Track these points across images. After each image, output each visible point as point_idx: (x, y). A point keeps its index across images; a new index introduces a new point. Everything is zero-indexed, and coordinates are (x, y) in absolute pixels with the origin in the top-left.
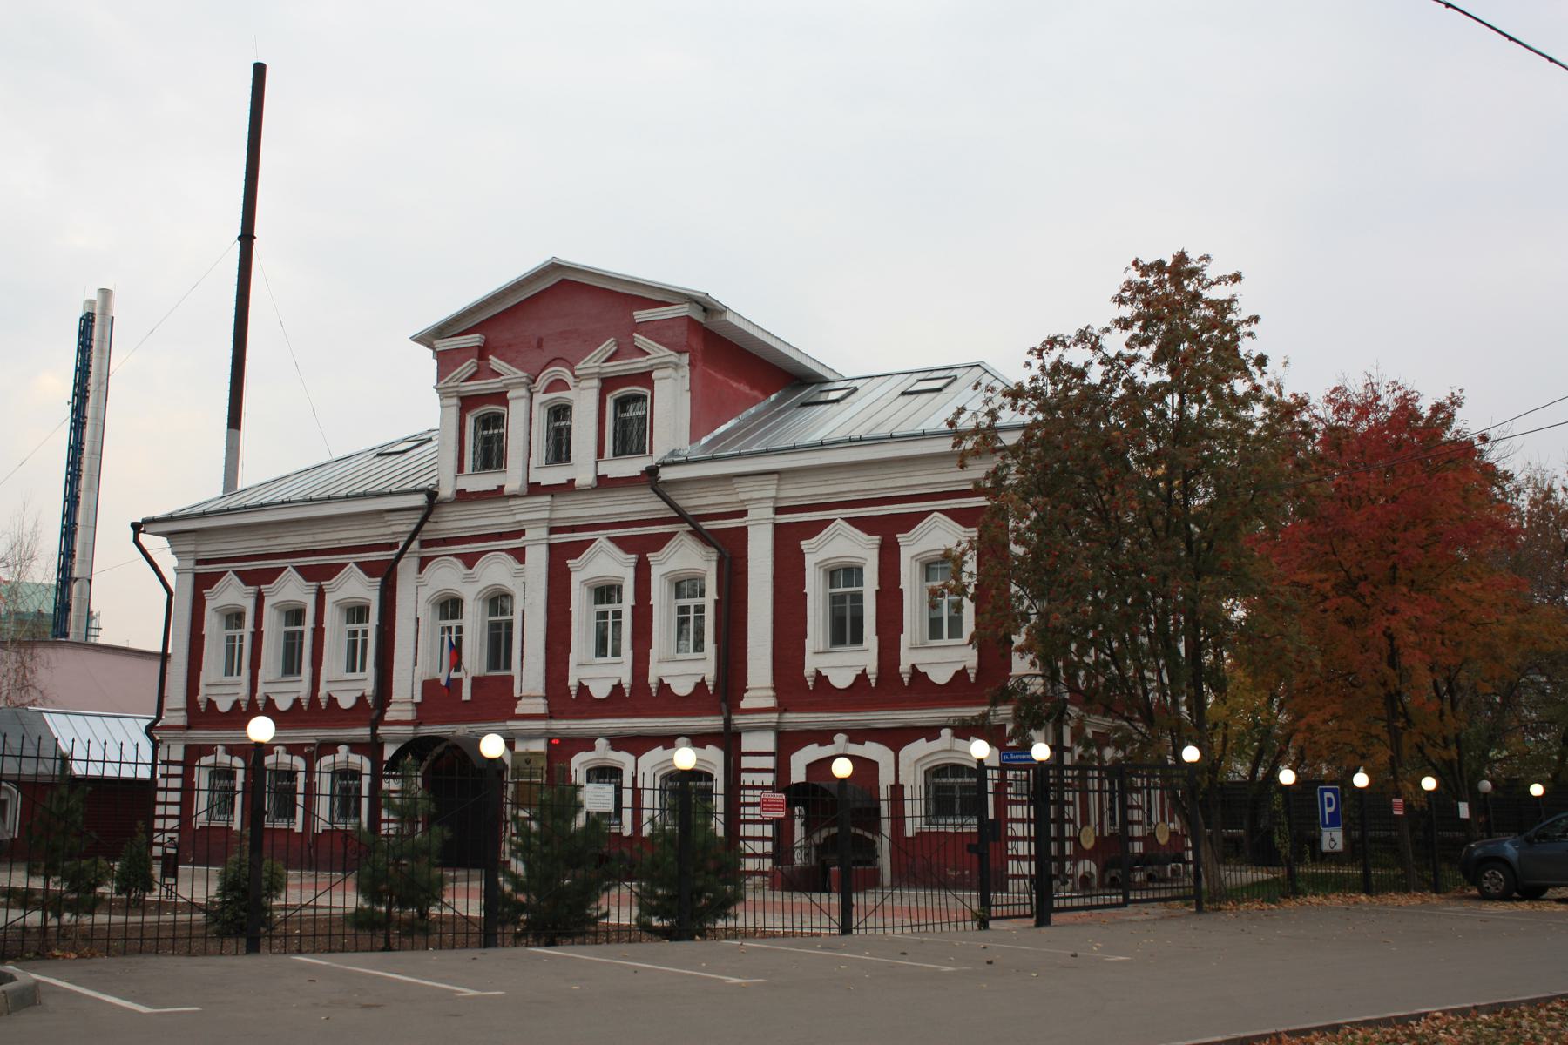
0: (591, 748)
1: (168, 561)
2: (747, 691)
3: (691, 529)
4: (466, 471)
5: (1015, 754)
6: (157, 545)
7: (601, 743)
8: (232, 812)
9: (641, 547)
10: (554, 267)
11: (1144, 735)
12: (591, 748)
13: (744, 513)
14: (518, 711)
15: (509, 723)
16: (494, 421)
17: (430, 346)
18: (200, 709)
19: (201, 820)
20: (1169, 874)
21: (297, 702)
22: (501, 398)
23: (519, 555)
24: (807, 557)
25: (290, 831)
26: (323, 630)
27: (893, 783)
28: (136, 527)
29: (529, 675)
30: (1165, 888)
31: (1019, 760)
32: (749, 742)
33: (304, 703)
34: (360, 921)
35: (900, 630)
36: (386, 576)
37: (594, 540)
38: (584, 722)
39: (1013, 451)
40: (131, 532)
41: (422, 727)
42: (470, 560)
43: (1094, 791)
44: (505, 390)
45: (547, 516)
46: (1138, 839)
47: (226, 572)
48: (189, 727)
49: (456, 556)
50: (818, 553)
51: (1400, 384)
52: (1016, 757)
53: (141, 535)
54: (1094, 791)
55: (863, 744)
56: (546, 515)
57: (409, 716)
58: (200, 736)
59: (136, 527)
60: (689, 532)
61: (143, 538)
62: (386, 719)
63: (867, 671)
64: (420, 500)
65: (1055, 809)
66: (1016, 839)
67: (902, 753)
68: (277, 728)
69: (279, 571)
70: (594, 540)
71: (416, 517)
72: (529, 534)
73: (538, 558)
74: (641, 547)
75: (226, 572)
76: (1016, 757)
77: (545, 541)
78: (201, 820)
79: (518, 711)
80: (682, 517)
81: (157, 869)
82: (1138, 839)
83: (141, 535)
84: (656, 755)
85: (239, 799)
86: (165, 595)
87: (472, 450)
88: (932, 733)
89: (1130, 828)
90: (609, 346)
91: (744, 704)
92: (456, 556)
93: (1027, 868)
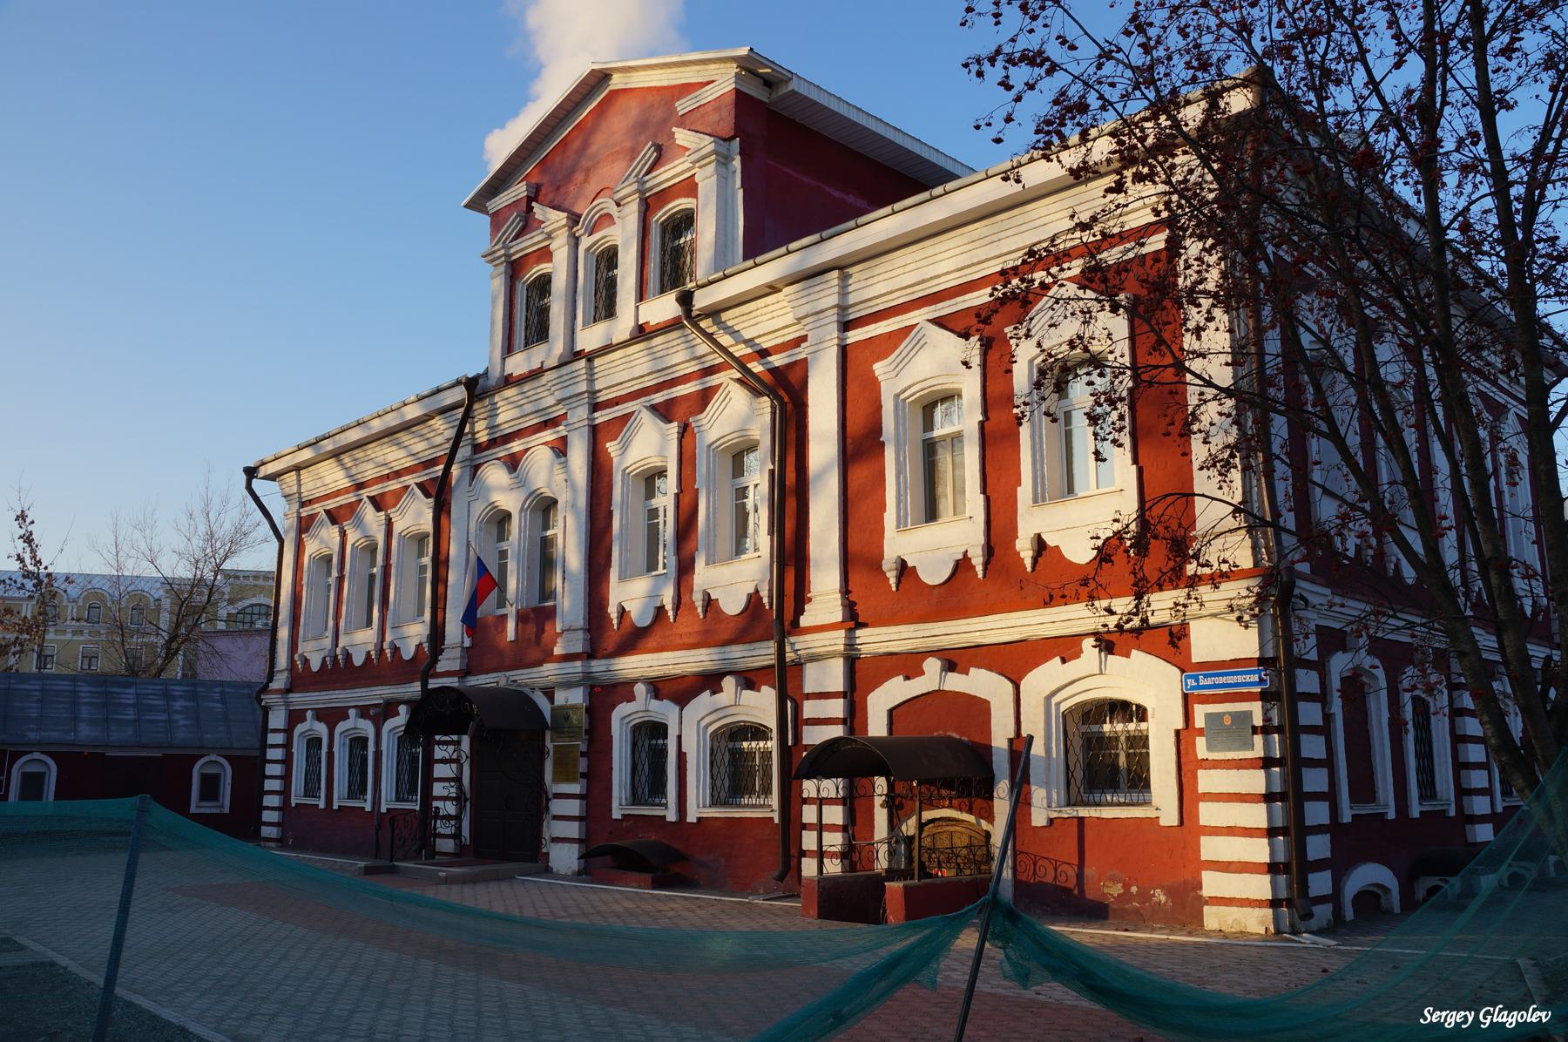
0: (631, 698)
3: (739, 375)
5: (1206, 676)
11: (1498, 564)
17: (484, 211)
18: (1525, 614)
20: (1552, 873)
27: (1012, 735)
28: (251, 473)
29: (569, 600)
30: (1422, 382)
31: (1215, 686)
32: (814, 678)
39: (1215, 201)
40: (244, 477)
41: (469, 678)
44: (546, 243)
46: (1483, 819)
52: (1209, 681)
55: (1128, 655)
57: (456, 666)
59: (251, 473)
60: (739, 381)
61: (257, 484)
62: (438, 670)
63: (969, 555)
64: (460, 394)
67: (1025, 684)
76: (1209, 681)
82: (1483, 819)
84: (705, 700)
86: (276, 544)
87: (523, 325)
88: (1066, 647)
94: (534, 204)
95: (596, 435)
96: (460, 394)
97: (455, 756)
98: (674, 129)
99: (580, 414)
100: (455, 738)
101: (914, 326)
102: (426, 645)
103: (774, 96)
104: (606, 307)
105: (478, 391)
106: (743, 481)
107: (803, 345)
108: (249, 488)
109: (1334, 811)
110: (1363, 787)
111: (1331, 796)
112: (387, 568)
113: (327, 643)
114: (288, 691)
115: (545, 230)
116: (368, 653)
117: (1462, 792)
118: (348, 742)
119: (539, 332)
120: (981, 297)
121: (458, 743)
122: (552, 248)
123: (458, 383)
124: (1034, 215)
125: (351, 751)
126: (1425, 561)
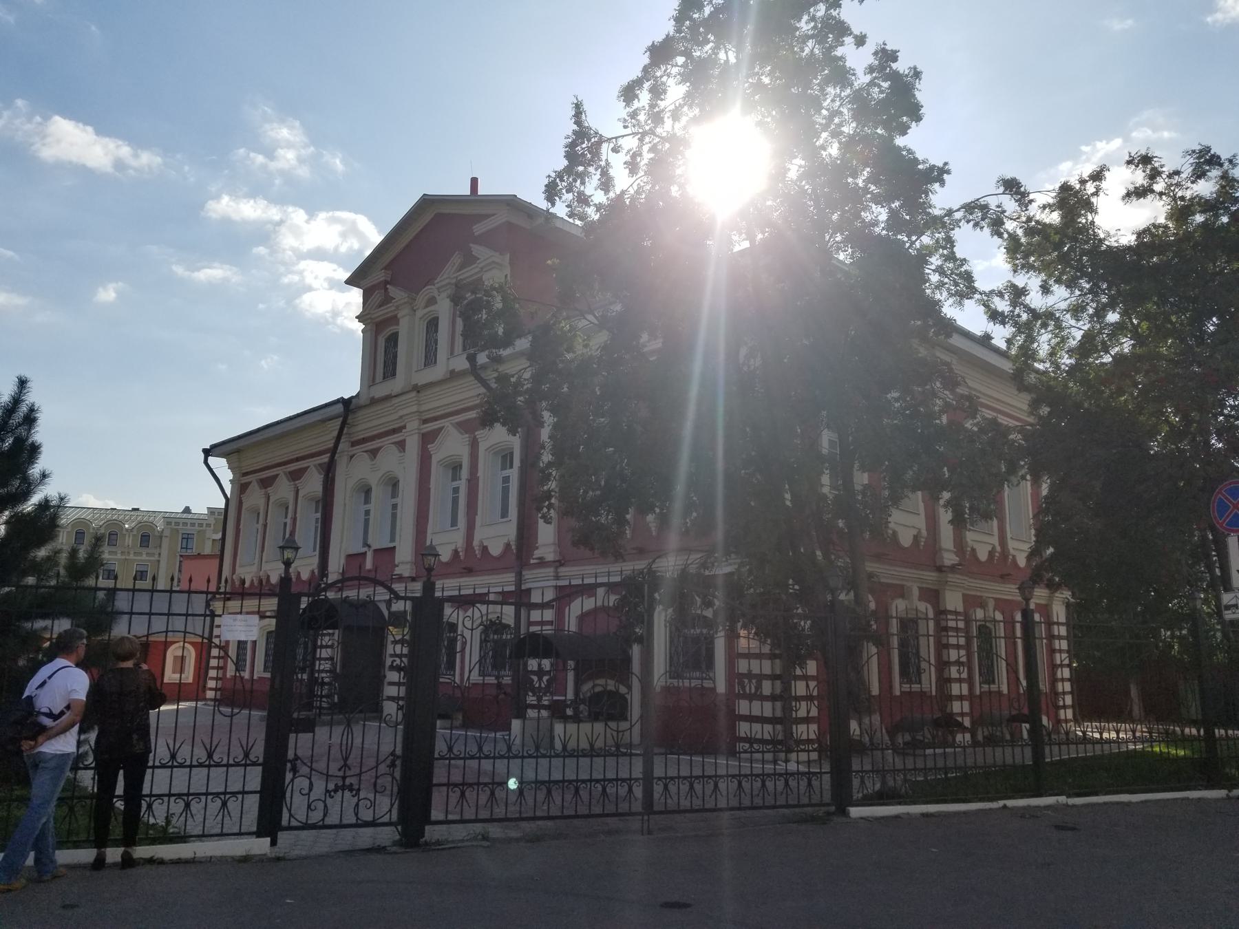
1: (226, 475)
2: (537, 548)
4: (377, 381)
6: (219, 463)
16: (393, 340)
21: (456, 552)
22: (394, 320)
23: (401, 445)
24: (433, 457)
26: (478, 479)
35: (476, 514)
37: (441, 429)
38: (501, 576)
40: (202, 456)
42: (374, 453)
43: (484, 680)
45: (415, 410)
47: (308, 467)
53: (210, 458)
54: (484, 680)
56: (414, 409)
59: (207, 452)
65: (973, 632)
70: (441, 429)
71: (338, 422)
72: (409, 427)
73: (413, 443)
75: (308, 467)
77: (417, 431)
81: (90, 760)
83: (210, 458)
90: (456, 259)
92: (366, 452)
94: (388, 286)
95: (427, 439)
96: (340, 407)
97: (330, 643)
98: (471, 245)
99: (413, 425)
100: (331, 631)
101: (443, 427)
102: (316, 571)
103: (612, 195)
104: (430, 358)
105: (352, 407)
106: (398, 500)
107: (404, 431)
108: (206, 462)
109: (971, 688)
110: (989, 675)
111: (970, 680)
112: (294, 520)
113: (254, 569)
114: (560, 563)
115: (395, 304)
116: (253, 580)
117: (944, 681)
118: (265, 632)
119: (390, 370)
120: (472, 415)
121: (333, 634)
122: (399, 316)
123: (962, 208)
124: (393, 402)
125: (267, 639)
126: (28, 625)
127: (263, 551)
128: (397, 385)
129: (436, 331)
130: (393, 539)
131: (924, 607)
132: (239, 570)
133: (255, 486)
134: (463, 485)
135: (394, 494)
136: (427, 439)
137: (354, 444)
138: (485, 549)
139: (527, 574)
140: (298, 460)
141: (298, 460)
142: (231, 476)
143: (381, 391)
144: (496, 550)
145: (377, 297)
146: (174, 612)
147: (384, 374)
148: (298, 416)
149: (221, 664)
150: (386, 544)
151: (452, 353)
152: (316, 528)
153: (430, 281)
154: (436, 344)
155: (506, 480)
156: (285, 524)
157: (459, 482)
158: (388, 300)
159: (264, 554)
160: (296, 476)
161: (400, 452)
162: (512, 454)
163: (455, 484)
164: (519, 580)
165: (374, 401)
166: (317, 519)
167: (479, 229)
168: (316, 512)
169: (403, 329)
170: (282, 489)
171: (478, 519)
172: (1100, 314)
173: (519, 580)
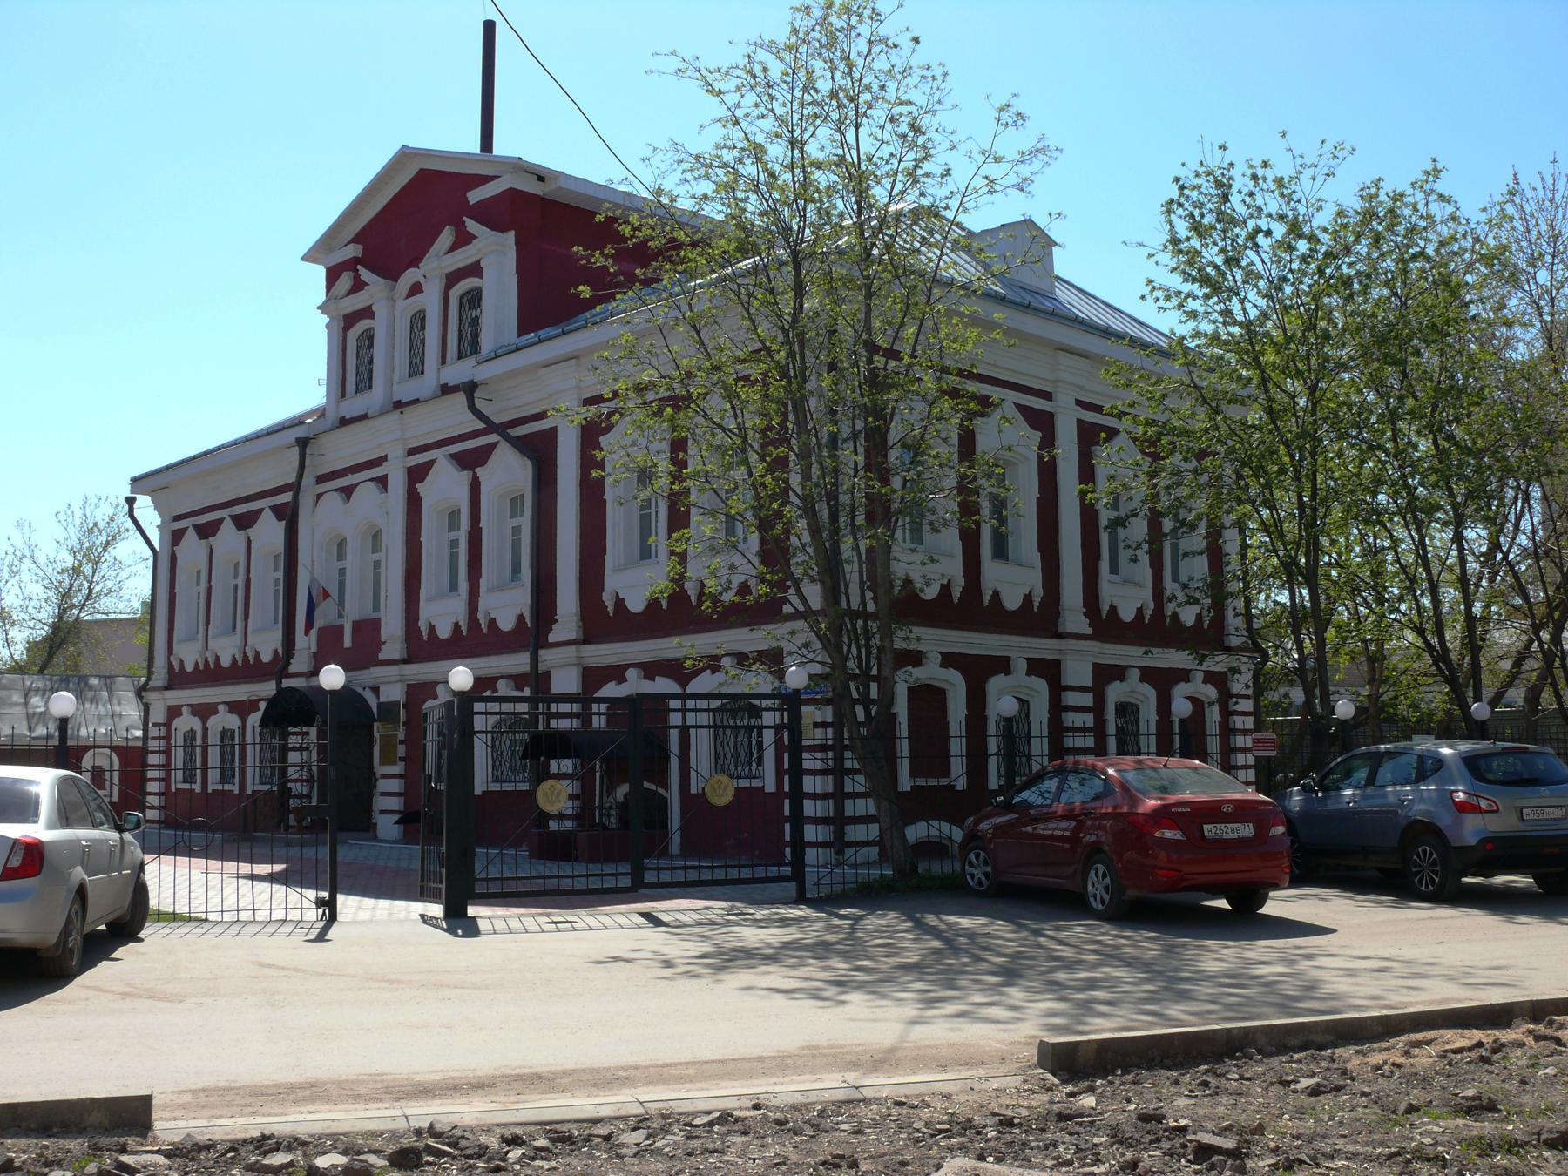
7: (631, 674)
8: (760, 761)
9: (471, 461)
10: (405, 155)
12: (622, 679)
13: (384, 459)
14: (381, 657)
15: (373, 670)
19: (482, 781)
23: (382, 481)
25: (192, 791)
33: (464, 629)
34: (914, 939)
36: (289, 515)
42: (347, 492)
48: (405, 661)
49: (372, 480)
50: (617, 450)
51: (63, 508)
58: (604, 653)
66: (152, 780)
68: (346, 670)
69: (431, 463)
73: (398, 482)
74: (471, 461)
78: (906, 784)
79: (381, 657)
80: (491, 427)
85: (1177, 730)
89: (1233, 756)
90: (446, 237)
91: (552, 638)
92: (372, 480)
93: (395, 804)
95: (417, 475)
104: (416, 368)
127: (207, 622)
128: (376, 396)
129: (423, 328)
130: (376, 608)
131: (1211, 692)
132: (484, 603)
133: (191, 535)
134: (462, 535)
135: (376, 548)
136: (417, 475)
137: (321, 479)
138: (492, 622)
139: (545, 654)
140: (247, 499)
141: (247, 499)
142: (158, 521)
143: (352, 407)
144: (506, 624)
145: (345, 281)
146: (1069, 630)
147: (357, 385)
148: (168, 468)
149: (162, 776)
150: (368, 613)
151: (343, 395)
152: (277, 592)
153: (415, 262)
154: (423, 346)
155: (516, 530)
156: (236, 587)
157: (520, 519)
158: (359, 285)
159: (250, 620)
160: (244, 522)
161: (381, 492)
162: (522, 496)
163: (453, 535)
164: (535, 660)
165: (344, 422)
166: (277, 581)
167: (475, 196)
168: (276, 570)
169: (379, 324)
170: (229, 539)
171: (483, 582)
172: (866, 419)
173: (535, 660)
